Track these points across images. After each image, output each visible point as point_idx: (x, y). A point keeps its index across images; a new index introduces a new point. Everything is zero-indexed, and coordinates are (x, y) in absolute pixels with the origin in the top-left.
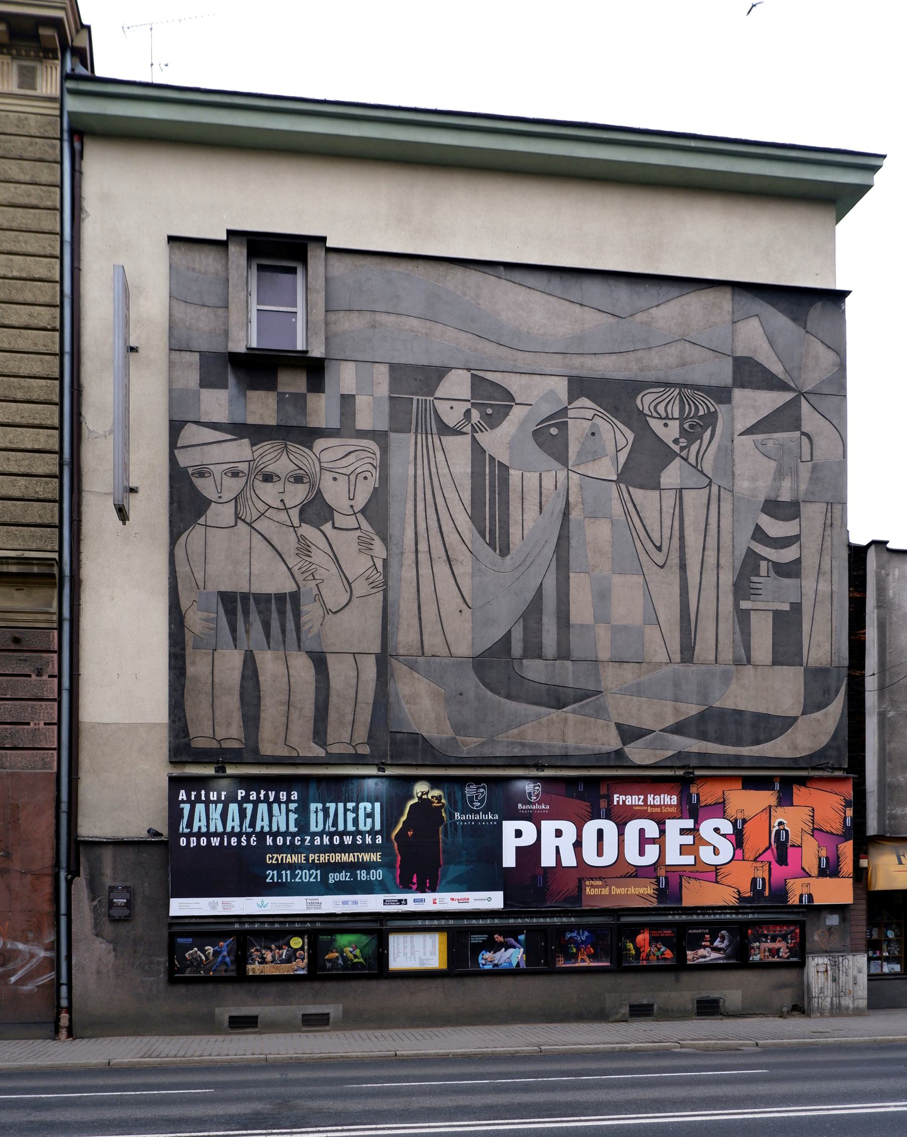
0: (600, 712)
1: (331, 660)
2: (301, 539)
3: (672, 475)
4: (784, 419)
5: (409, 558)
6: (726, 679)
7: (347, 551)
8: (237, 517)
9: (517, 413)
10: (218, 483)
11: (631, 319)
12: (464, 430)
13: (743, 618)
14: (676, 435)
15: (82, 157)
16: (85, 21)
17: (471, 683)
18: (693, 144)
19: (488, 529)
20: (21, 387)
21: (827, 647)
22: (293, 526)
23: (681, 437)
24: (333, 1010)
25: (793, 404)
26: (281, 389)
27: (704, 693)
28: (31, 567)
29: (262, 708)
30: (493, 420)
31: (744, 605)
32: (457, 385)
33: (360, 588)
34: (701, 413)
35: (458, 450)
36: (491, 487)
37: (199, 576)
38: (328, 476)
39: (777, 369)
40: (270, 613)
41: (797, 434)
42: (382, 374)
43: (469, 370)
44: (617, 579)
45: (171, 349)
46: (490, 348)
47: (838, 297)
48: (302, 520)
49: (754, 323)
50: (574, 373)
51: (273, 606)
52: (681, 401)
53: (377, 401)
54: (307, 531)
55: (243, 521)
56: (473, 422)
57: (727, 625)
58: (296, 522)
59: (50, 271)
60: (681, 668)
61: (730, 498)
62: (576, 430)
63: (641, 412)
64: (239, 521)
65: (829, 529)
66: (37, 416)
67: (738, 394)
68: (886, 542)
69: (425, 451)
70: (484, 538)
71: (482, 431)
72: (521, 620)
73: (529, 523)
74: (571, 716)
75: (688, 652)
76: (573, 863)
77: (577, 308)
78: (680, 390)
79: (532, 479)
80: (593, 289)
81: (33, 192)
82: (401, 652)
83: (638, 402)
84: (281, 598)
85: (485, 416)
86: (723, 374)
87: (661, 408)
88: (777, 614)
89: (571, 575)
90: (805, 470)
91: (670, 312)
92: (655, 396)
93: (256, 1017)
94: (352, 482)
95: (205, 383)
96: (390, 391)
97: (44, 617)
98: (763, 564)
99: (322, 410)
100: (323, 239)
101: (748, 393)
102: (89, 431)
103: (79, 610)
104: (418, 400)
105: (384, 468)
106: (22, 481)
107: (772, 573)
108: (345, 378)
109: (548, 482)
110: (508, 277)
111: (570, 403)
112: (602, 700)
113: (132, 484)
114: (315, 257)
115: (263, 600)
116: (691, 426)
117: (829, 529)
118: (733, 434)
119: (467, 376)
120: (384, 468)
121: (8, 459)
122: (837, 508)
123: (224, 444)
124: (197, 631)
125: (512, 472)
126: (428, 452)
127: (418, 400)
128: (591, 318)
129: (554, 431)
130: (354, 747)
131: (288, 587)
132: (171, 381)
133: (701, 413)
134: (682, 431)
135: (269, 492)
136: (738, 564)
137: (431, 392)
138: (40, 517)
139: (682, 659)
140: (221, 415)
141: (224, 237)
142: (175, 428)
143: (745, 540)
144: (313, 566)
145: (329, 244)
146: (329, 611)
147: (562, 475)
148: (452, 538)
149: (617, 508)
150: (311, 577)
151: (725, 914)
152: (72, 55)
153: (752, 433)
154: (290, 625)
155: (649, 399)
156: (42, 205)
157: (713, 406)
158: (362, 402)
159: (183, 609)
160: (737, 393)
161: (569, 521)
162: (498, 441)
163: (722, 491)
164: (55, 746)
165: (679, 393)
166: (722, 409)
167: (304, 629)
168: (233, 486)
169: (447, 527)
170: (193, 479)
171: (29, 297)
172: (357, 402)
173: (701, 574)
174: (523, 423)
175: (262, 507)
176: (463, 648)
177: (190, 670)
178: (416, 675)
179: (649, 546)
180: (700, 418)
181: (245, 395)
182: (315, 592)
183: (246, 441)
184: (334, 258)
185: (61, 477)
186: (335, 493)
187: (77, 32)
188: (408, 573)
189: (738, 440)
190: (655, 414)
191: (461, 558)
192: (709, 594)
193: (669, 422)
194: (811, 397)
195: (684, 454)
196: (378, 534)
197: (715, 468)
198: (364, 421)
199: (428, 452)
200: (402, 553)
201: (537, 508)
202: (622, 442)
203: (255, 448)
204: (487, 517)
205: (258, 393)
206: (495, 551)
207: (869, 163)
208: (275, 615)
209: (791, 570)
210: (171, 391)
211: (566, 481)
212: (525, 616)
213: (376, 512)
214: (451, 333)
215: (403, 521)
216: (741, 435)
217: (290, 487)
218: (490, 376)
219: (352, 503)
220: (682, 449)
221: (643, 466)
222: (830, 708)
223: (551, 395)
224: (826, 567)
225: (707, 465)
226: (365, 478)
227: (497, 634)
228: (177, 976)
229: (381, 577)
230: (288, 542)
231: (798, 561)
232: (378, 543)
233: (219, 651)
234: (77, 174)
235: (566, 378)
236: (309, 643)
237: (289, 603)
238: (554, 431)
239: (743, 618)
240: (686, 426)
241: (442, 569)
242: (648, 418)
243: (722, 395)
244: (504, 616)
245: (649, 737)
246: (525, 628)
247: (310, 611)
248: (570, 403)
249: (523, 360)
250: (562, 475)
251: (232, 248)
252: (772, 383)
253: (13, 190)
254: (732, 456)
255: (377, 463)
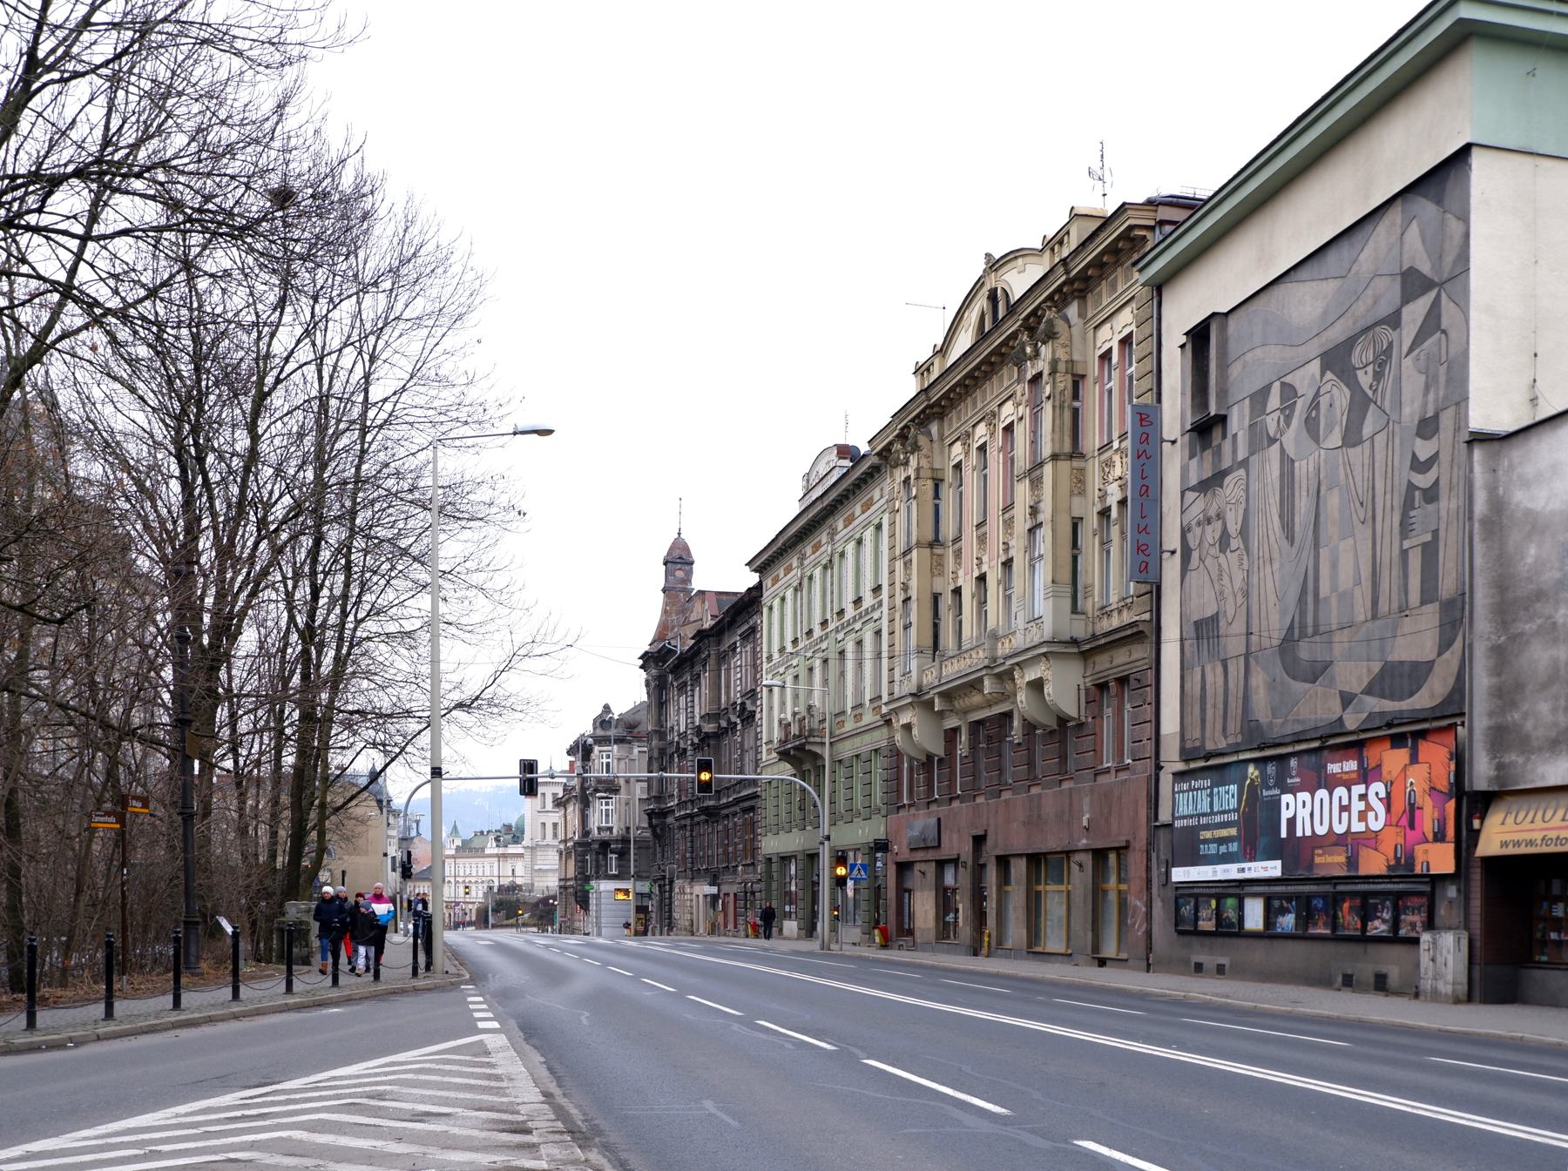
18: (1350, 83)
76: (1308, 833)
143: (1404, 474)
228: (1186, 930)
254: (670, 911)
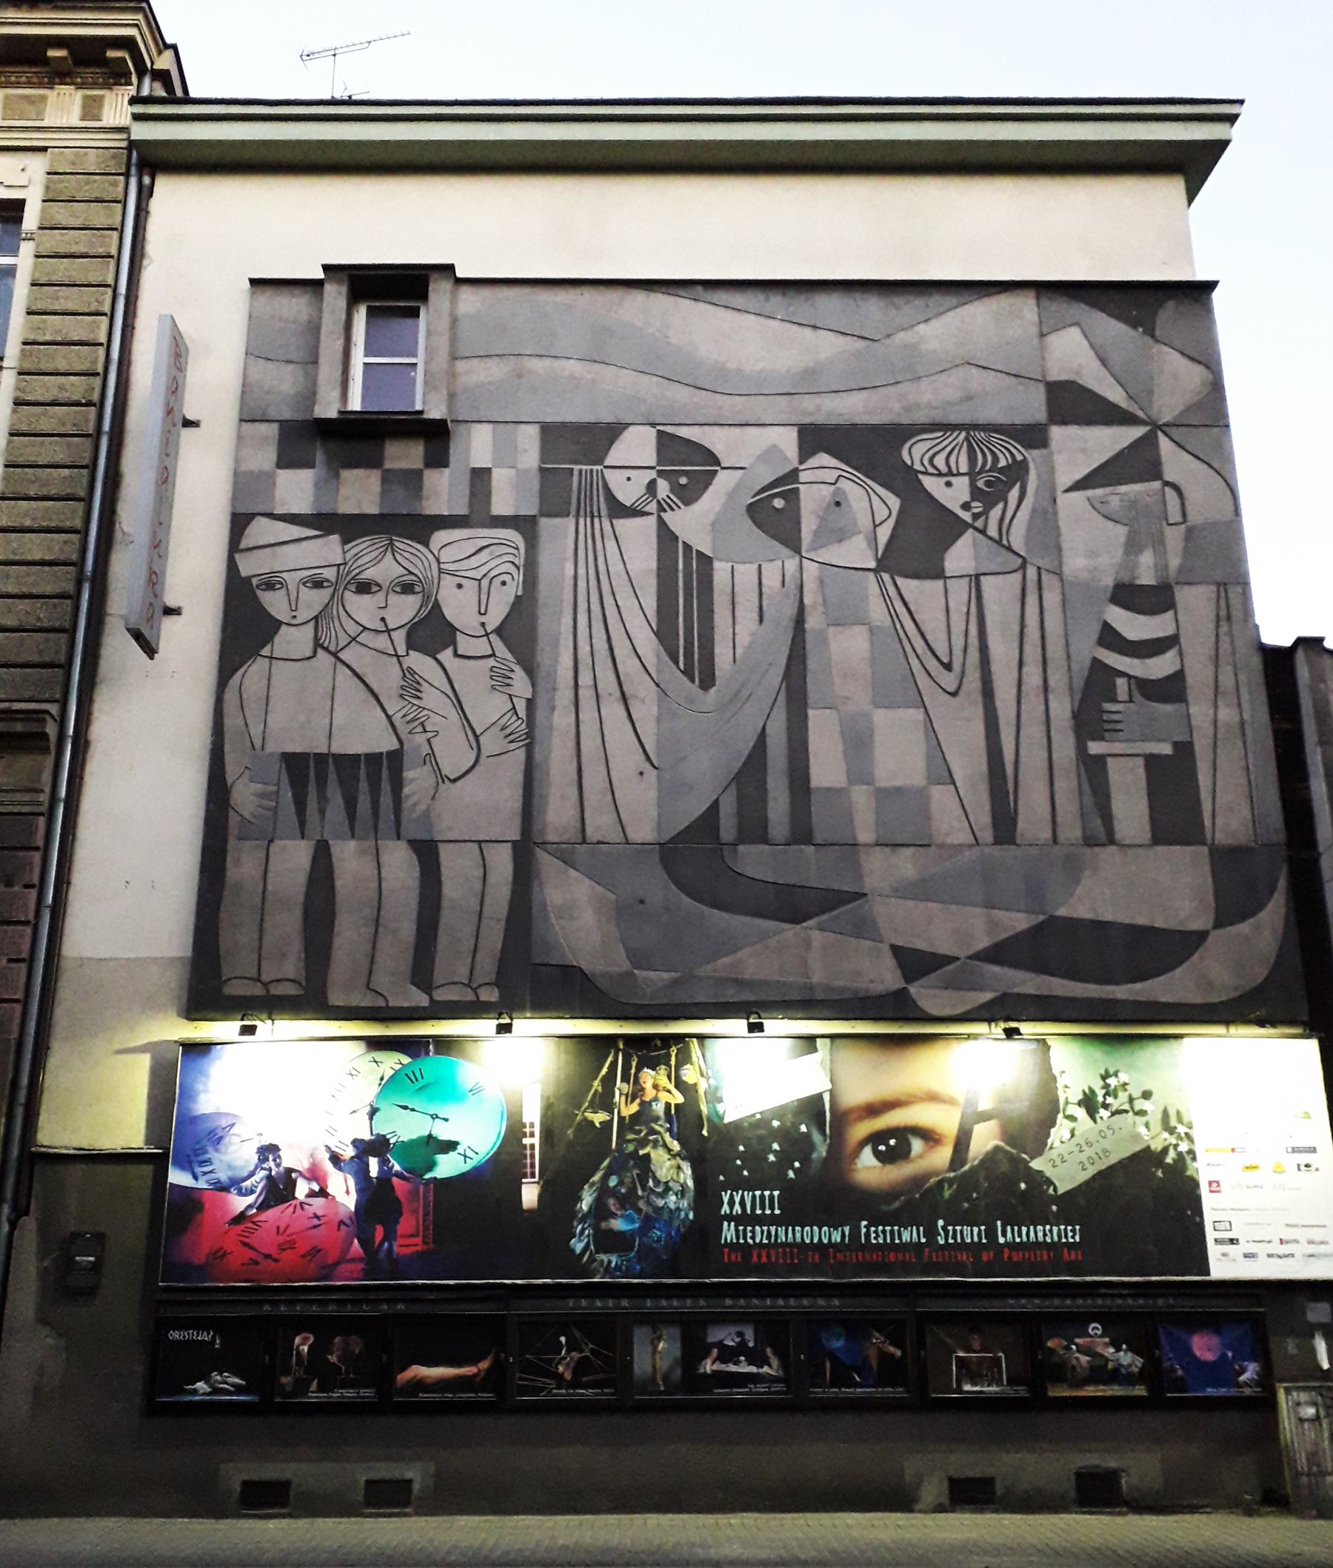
0: (864, 929)
1: (445, 852)
2: (408, 673)
3: (960, 557)
4: (1137, 464)
5: (564, 697)
6: (1073, 869)
7: (476, 689)
8: (318, 644)
9: (724, 481)
10: (293, 597)
11: (888, 342)
12: (646, 509)
13: (1094, 770)
14: (966, 497)
15: (151, 195)
16: (169, 41)
17: (656, 886)
19: (681, 651)
20: (37, 479)
21: (1246, 812)
22: (396, 655)
23: (973, 499)
24: (416, 1474)
25: (1145, 447)
26: (388, 465)
27: (1035, 895)
28: (12, 724)
29: (336, 929)
30: (688, 494)
31: (1095, 748)
32: (637, 447)
33: (491, 743)
34: (1002, 463)
35: (638, 540)
36: (685, 586)
37: (256, 730)
38: (448, 582)
39: (1115, 394)
40: (352, 786)
41: (1157, 485)
42: (529, 439)
43: (653, 425)
44: (880, 716)
45: (241, 420)
46: (682, 395)
47: (1200, 291)
48: (411, 646)
49: (1074, 334)
50: (807, 420)
51: (363, 773)
52: (970, 448)
53: (522, 474)
54: (418, 661)
55: (326, 649)
56: (660, 497)
57: (1067, 783)
58: (401, 649)
59: (93, 332)
60: (996, 851)
61: (1057, 583)
62: (812, 499)
63: (910, 469)
64: (320, 652)
65: (1224, 624)
66: (54, 517)
67: (1057, 433)
68: (1321, 640)
69: (590, 541)
70: (677, 663)
71: (672, 509)
72: (734, 785)
73: (741, 637)
74: (816, 936)
75: (1005, 824)
77: (808, 332)
78: (968, 433)
79: (746, 573)
80: (828, 304)
81: (83, 238)
82: (551, 837)
83: (905, 453)
84: (374, 759)
85: (677, 489)
86: (1033, 407)
87: (940, 461)
88: (1151, 760)
89: (811, 713)
90: (1174, 537)
91: (942, 331)
92: (928, 444)
93: (286, 1485)
94: (485, 589)
95: (285, 461)
96: (543, 460)
97: (26, 797)
98: (1121, 683)
99: (443, 491)
100: (450, 268)
101: (1073, 430)
102: (124, 533)
103: (81, 785)
104: (581, 471)
105: (530, 567)
106: (22, 605)
107: (1137, 697)
108: (477, 446)
109: (772, 580)
110: (709, 299)
111: (801, 462)
112: (866, 907)
113: (171, 601)
114: (439, 291)
115: (348, 763)
116: (988, 484)
117: (1224, 624)
118: (1053, 490)
119: (651, 433)
120: (530, 567)
121: (8, 576)
122: (1234, 592)
123: (304, 543)
124: (246, 814)
125: (717, 565)
126: (596, 559)
127: (581, 471)
128: (827, 346)
129: (779, 503)
130: (475, 990)
131: (386, 743)
132: (237, 461)
133: (1002, 463)
134: (976, 493)
135: (362, 608)
136: (1079, 683)
137: (600, 462)
138: (40, 653)
139: (995, 837)
140: (302, 506)
141: (320, 275)
142: (239, 523)
144: (425, 712)
145: (460, 274)
146: (444, 778)
147: (792, 565)
148: (628, 665)
149: (877, 612)
150: (420, 729)
151: (1113, 1296)
152: (153, 80)
153: (1084, 488)
154: (386, 800)
155: (919, 449)
156: (92, 252)
157: (1020, 452)
158: (501, 479)
159: (229, 781)
160: (1056, 432)
161: (804, 631)
162: (692, 524)
163: (1045, 576)
164: (20, 995)
165: (967, 439)
166: (1033, 456)
167: (407, 805)
168: (313, 600)
169: (622, 650)
170: (259, 592)
171: (62, 366)
172: (494, 482)
173: (1019, 702)
174: (732, 495)
175: (352, 629)
176: (643, 832)
177: (232, 873)
178: (572, 872)
179: (932, 664)
180: (1001, 471)
181: (337, 476)
182: (426, 750)
183: (335, 538)
184: (465, 292)
185: (76, 598)
186: (458, 606)
187: (160, 52)
188: (562, 719)
189: (1063, 500)
190: (931, 470)
191: (642, 694)
192: (1033, 732)
193: (953, 479)
194: (1174, 432)
195: (979, 524)
196: (519, 663)
197: (1028, 538)
198: (502, 504)
199: (596, 559)
200: (555, 689)
201: (755, 616)
202: (881, 513)
203: (347, 547)
204: (681, 632)
205: (355, 472)
206: (693, 681)
207: (1225, 111)
208: (363, 786)
209: (1172, 689)
210: (236, 473)
211: (798, 574)
212: (738, 778)
213: (519, 633)
214: (627, 378)
215: (556, 644)
216: (1067, 491)
217: (395, 599)
218: (683, 432)
219: (483, 619)
220: (976, 516)
221: (918, 544)
222: (1263, 915)
223: (772, 453)
224: (1227, 679)
225: (1017, 538)
226: (504, 583)
227: (694, 808)
229: (524, 726)
230: (387, 678)
231: (1179, 676)
232: (519, 675)
233: (278, 843)
234: (143, 214)
235: (796, 429)
236: (410, 830)
237: (388, 767)
238: (779, 503)
239: (1094, 770)
240: (980, 484)
241: (613, 710)
242: (921, 476)
243: (1033, 436)
244: (707, 773)
245: (951, 967)
246: (740, 798)
247: (416, 779)
248: (801, 462)
249: (731, 406)
250: (792, 565)
251: (328, 288)
252: (1109, 414)
253: (59, 238)
255: (520, 561)
